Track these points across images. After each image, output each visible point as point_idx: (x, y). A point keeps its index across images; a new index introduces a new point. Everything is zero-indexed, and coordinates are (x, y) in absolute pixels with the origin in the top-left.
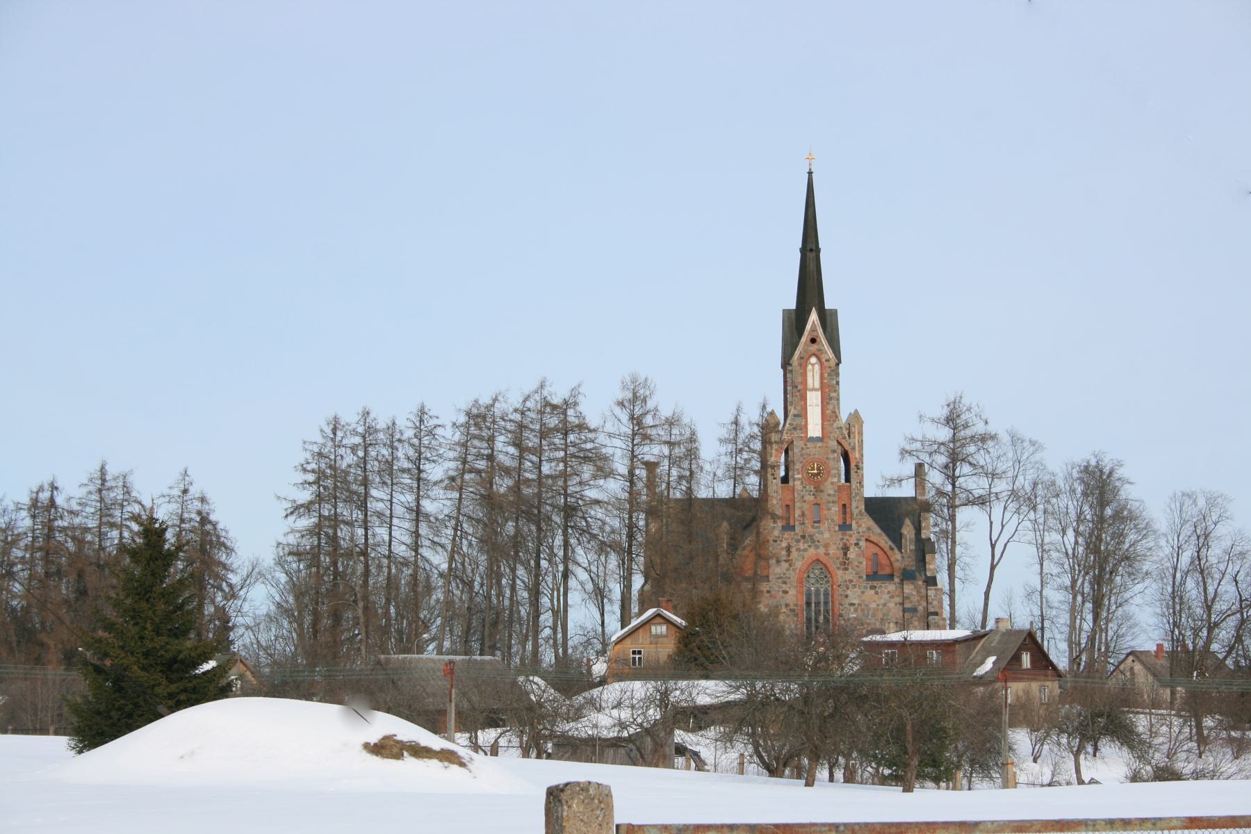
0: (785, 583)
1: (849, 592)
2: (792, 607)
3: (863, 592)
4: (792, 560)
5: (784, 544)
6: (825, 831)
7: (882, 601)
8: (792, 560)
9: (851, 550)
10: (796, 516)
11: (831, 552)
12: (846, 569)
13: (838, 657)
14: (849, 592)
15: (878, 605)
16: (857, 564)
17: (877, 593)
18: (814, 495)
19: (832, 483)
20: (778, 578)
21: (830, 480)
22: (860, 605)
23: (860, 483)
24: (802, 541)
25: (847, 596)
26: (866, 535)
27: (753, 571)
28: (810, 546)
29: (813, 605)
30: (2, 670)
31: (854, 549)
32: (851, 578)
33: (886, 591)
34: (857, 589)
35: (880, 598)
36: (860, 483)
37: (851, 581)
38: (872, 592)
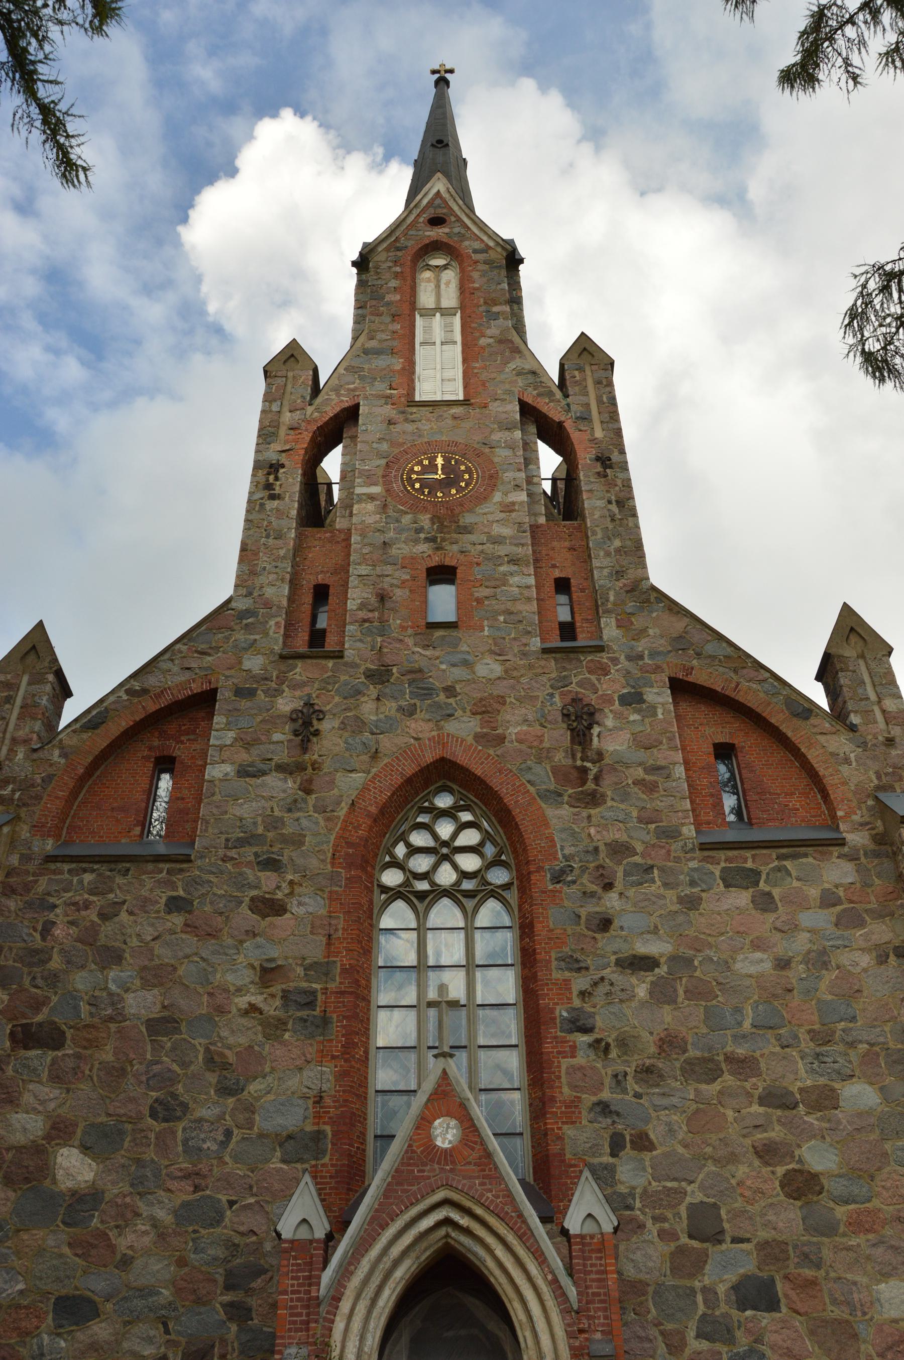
0: (272, 864)
1: (612, 901)
2: (298, 980)
3: (691, 903)
4: (316, 767)
5: (286, 704)
6: (901, 59)
7: (801, 943)
8: (316, 767)
9: (610, 722)
10: (351, 605)
11: (513, 731)
12: (594, 799)
13: (195, 1291)
14: (612, 901)
15: (783, 964)
16: (640, 773)
17: (765, 903)
18: (433, 540)
19: (508, 508)
20: (242, 843)
21: (497, 497)
22: (680, 962)
23: (620, 503)
24: (373, 691)
25: (605, 924)
26: (673, 665)
27: (499, 1072)
28: (410, 712)
29: (19, 701)
30: (3, 1342)
31: (618, 716)
32: (620, 836)
33: (814, 893)
34: (656, 888)
35: (789, 929)
36: (620, 503)
37: (619, 850)
38: (742, 898)
